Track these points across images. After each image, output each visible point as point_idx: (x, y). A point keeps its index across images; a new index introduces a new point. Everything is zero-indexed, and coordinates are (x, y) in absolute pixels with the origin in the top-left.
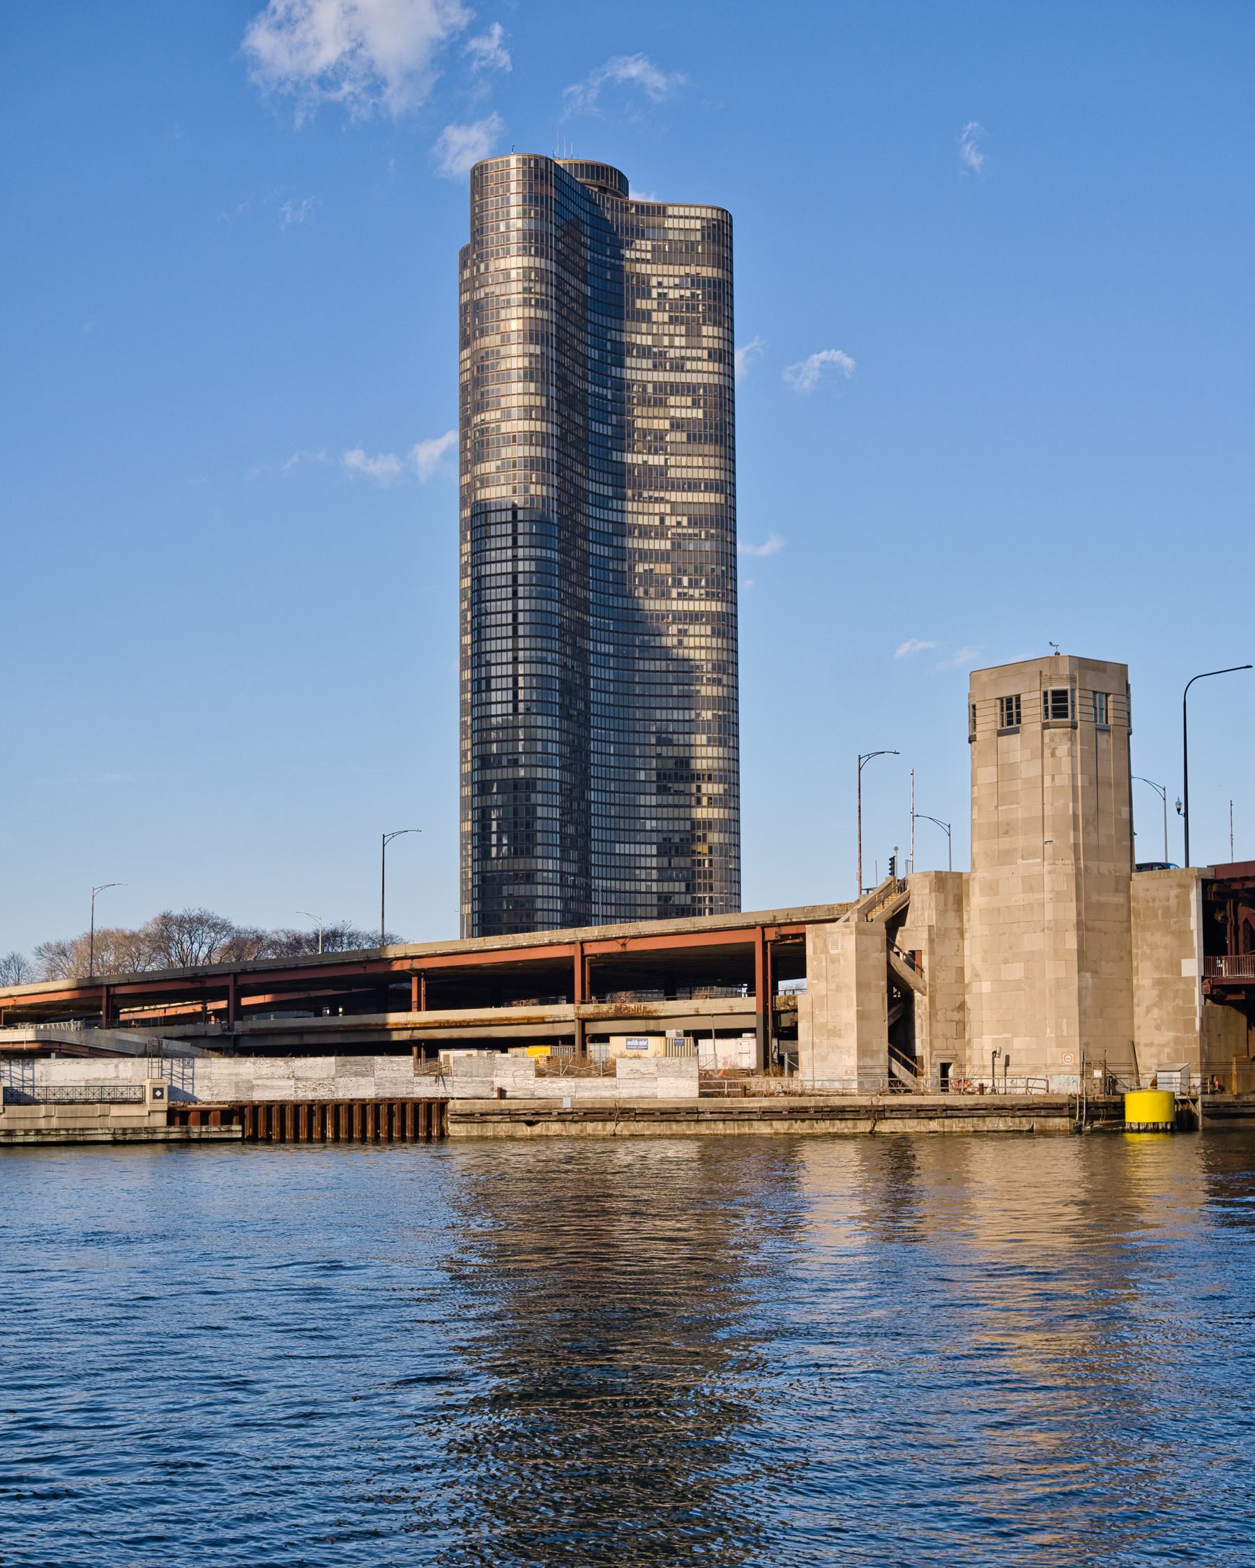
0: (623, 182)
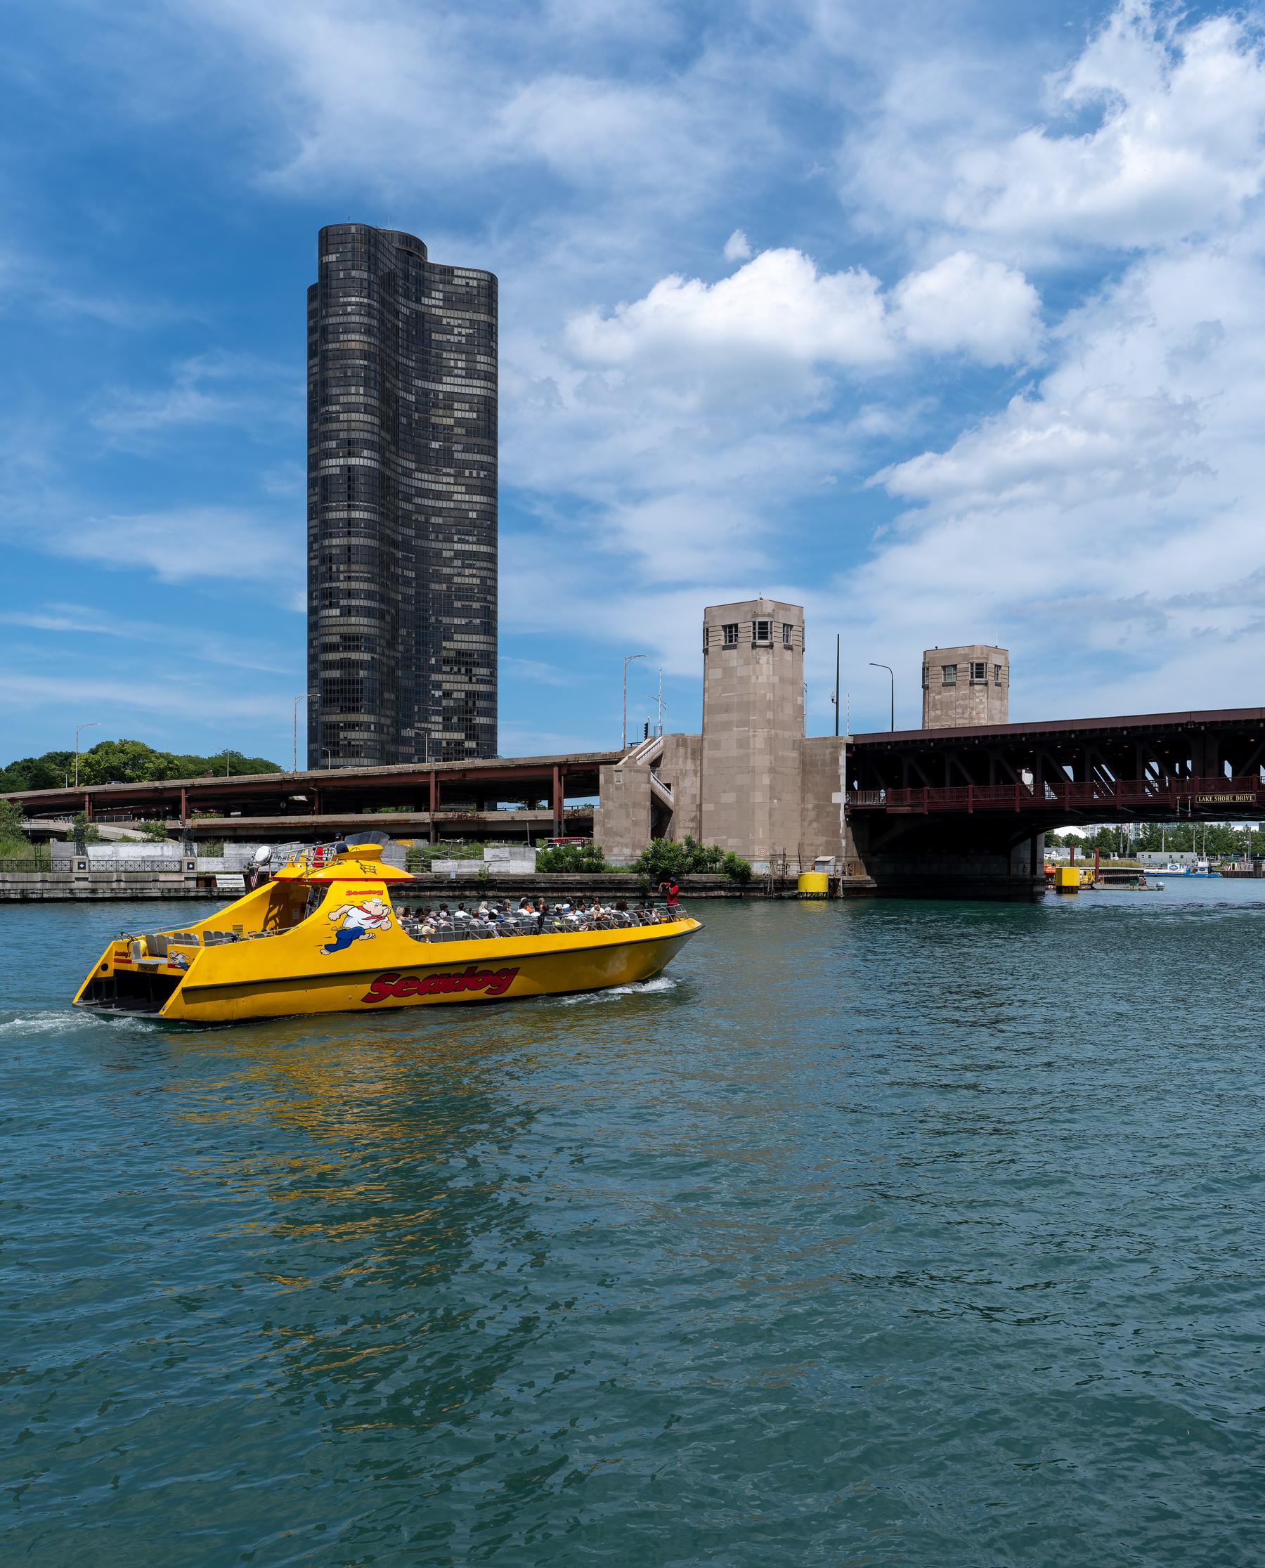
0: (421, 247)
